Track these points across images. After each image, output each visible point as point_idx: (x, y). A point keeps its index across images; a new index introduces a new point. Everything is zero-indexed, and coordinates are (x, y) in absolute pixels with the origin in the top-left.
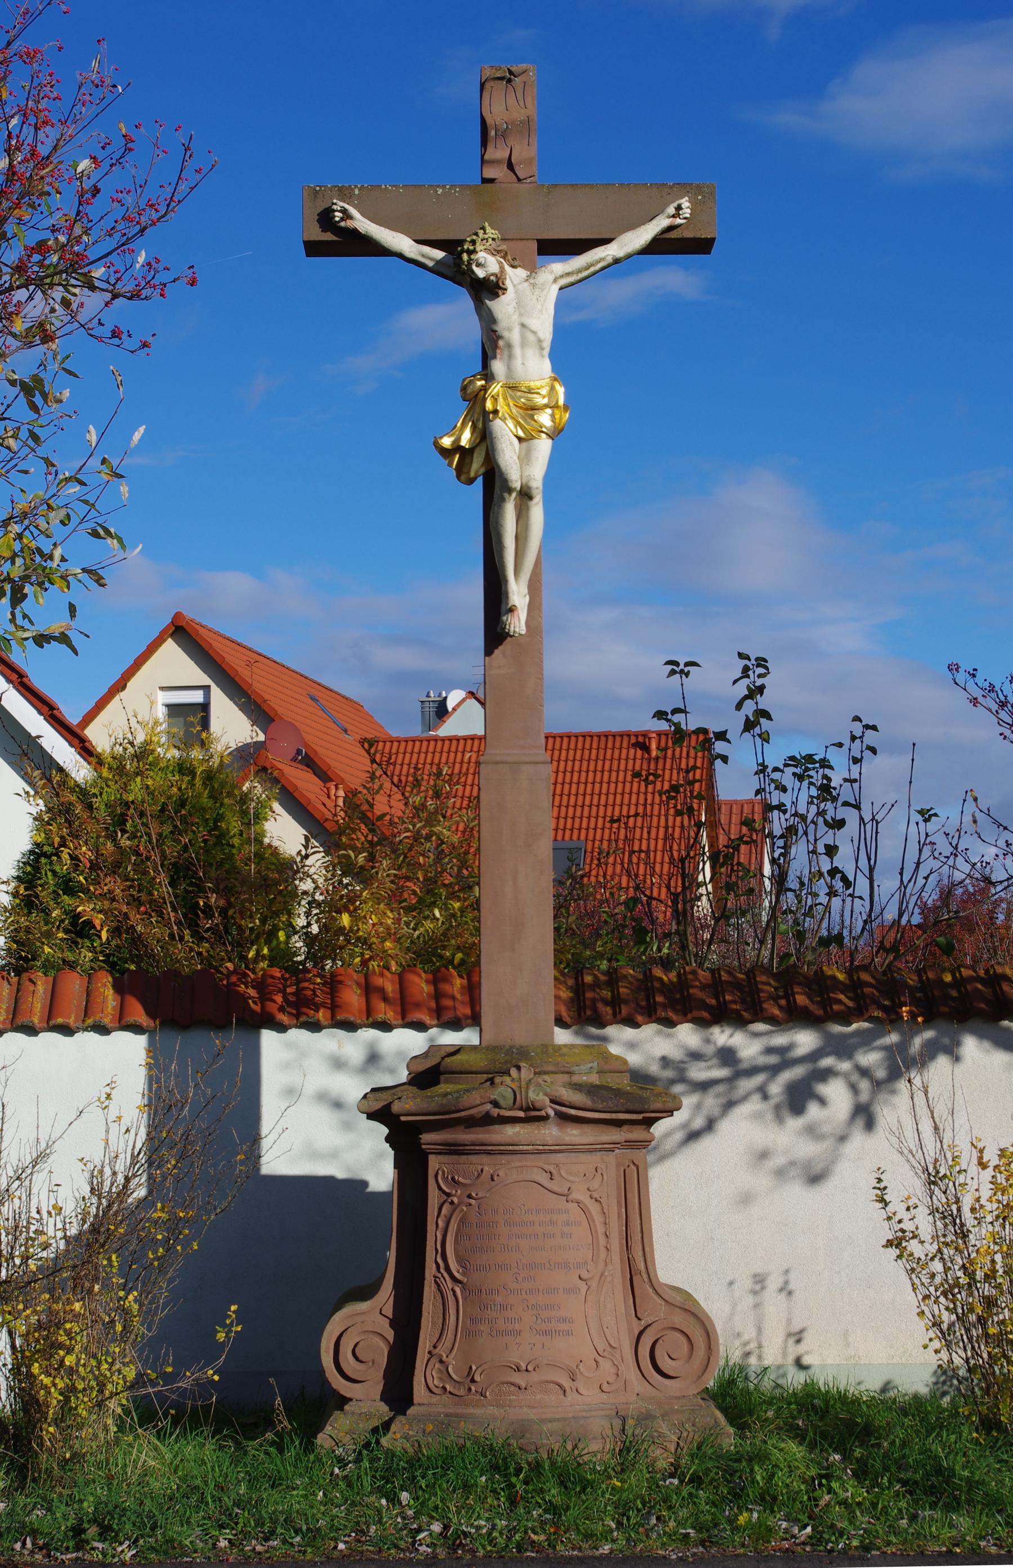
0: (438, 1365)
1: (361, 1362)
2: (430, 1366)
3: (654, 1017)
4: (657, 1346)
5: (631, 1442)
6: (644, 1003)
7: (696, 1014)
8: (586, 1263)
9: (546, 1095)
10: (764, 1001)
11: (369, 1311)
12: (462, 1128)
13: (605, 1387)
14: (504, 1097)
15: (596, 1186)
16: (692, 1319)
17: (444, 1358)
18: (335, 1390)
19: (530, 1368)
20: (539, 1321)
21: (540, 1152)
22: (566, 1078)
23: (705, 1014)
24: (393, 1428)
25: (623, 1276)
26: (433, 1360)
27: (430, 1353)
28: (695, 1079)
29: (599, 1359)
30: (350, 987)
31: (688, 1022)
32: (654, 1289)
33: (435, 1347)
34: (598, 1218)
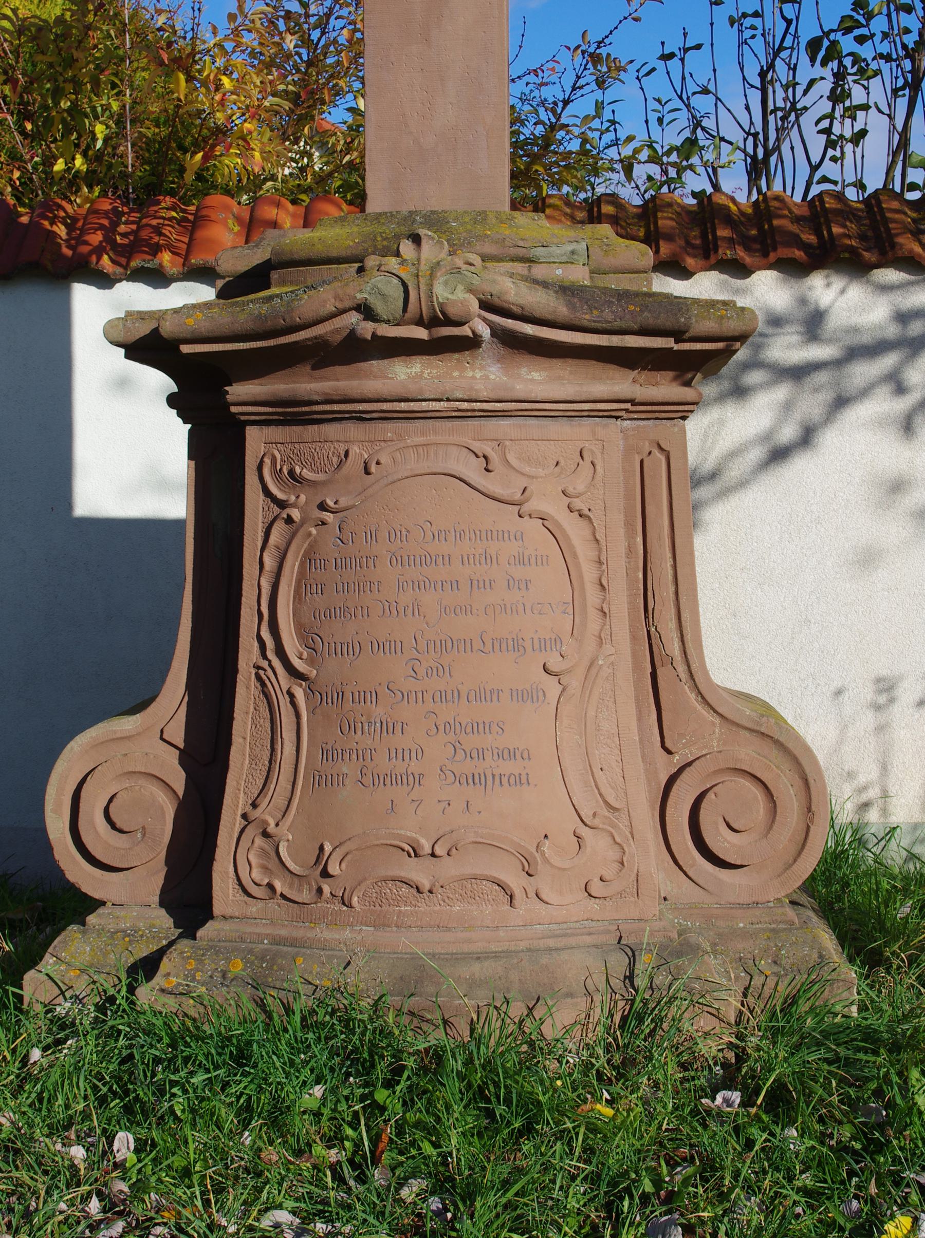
0: (259, 841)
1: (121, 831)
2: (245, 843)
3: (713, 260)
4: (704, 805)
5: (645, 1002)
6: (698, 242)
7: (784, 252)
8: (558, 640)
9: (471, 291)
10: (897, 235)
11: (139, 734)
12: (308, 368)
13: (597, 888)
14: (383, 296)
15: (581, 487)
16: (774, 754)
17: (271, 829)
18: (73, 885)
19: (438, 851)
20: (461, 754)
21: (463, 416)
22: (520, 268)
23: (798, 254)
24: (165, 965)
25: (637, 667)
26: (250, 832)
27: (244, 816)
28: (781, 362)
29: (584, 831)
30: (225, 224)
31: (769, 267)
32: (700, 693)
33: (254, 805)
34: (584, 552)
